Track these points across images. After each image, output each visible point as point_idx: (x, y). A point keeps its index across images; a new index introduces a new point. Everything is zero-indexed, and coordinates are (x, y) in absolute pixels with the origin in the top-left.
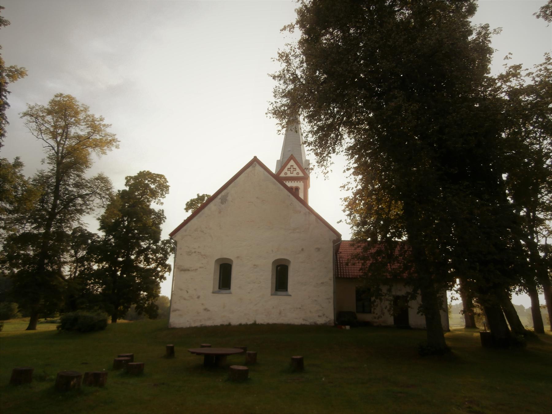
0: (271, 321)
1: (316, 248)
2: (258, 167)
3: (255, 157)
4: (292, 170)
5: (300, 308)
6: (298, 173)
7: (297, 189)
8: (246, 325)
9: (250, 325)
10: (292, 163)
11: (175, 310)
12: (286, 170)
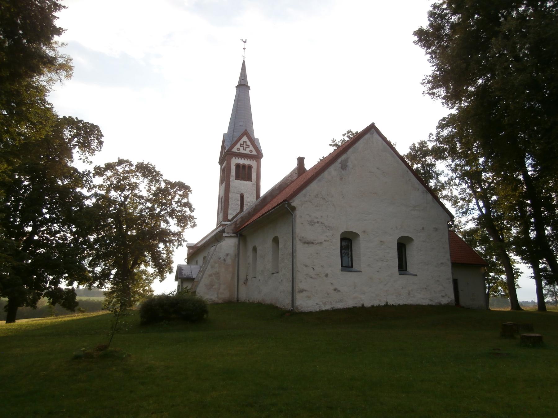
0: (401, 303)
1: (435, 228)
2: (376, 136)
3: (373, 124)
4: (245, 146)
5: (426, 288)
6: (251, 151)
7: (250, 167)
8: (379, 307)
9: (382, 306)
10: (245, 139)
11: (301, 291)
12: (238, 145)
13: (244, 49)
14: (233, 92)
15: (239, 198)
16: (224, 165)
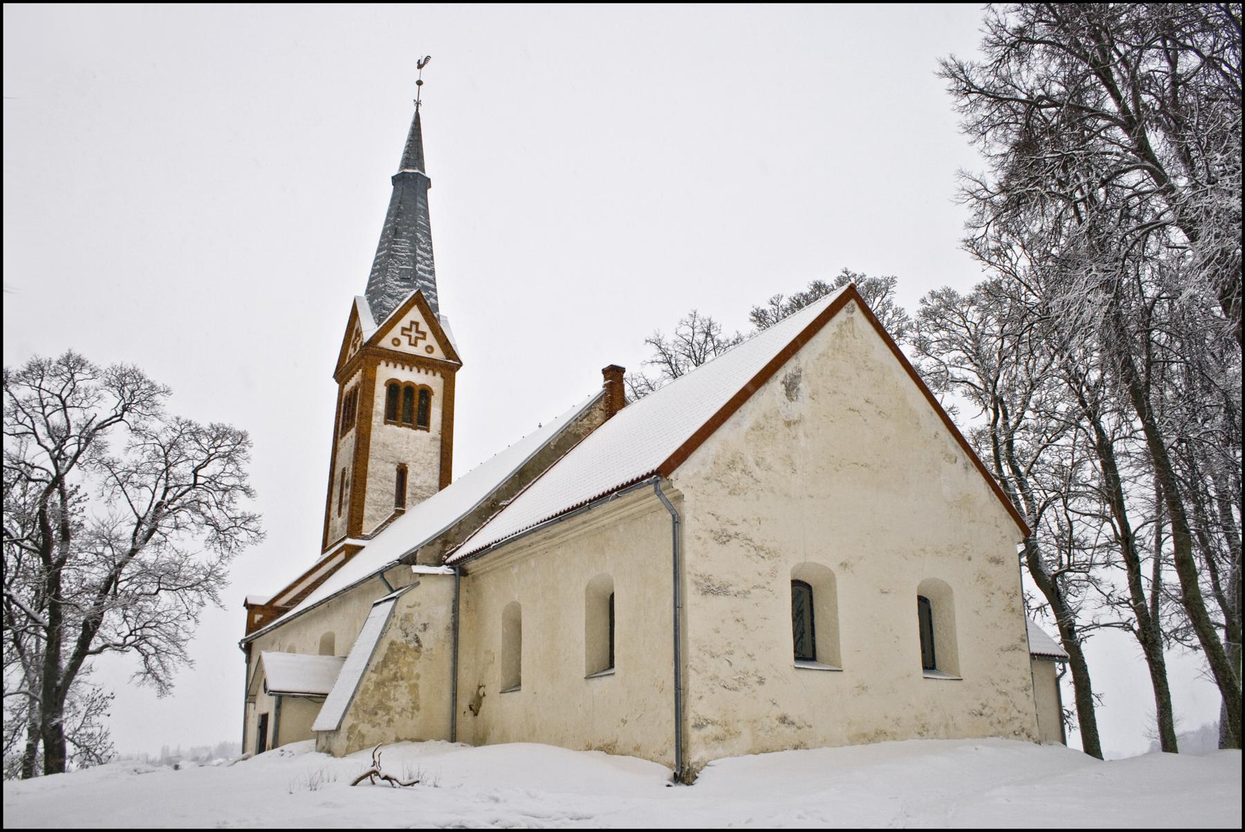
6: (430, 349)
7: (426, 392)
10: (415, 314)
12: (396, 332)
13: (419, 83)
14: (385, 193)
15: (395, 473)
16: (352, 383)
